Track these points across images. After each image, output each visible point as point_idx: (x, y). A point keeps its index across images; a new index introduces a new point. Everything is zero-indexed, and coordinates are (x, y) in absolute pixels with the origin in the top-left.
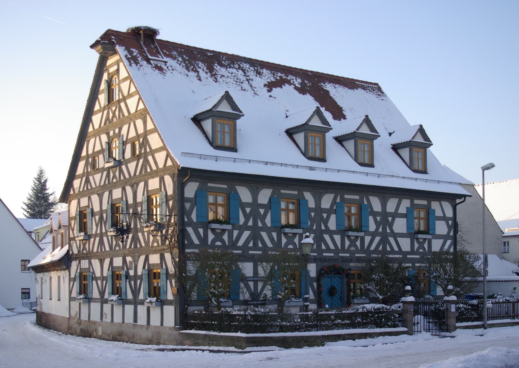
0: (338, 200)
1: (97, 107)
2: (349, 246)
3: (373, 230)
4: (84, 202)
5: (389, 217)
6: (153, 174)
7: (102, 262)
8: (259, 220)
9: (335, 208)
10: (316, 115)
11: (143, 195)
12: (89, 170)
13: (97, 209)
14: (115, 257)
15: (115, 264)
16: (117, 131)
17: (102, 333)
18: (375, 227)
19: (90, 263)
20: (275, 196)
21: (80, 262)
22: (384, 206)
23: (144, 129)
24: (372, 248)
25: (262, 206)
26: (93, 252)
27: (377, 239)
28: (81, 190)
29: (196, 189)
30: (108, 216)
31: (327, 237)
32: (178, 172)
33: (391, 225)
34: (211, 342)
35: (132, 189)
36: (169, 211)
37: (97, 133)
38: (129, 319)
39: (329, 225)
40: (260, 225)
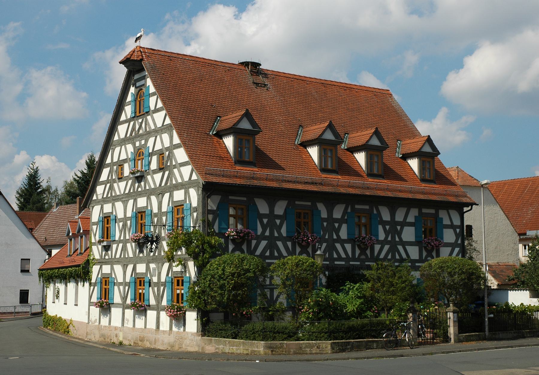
0: (349, 210)
1: (123, 118)
2: (360, 255)
3: (383, 239)
4: (107, 208)
5: (398, 226)
6: (178, 187)
7: (125, 267)
8: (275, 230)
9: (346, 218)
10: (328, 128)
11: (169, 205)
12: (114, 178)
13: (120, 215)
14: (138, 263)
15: (138, 271)
16: (143, 142)
17: (123, 338)
18: (384, 236)
19: (112, 269)
20: (290, 207)
21: (101, 268)
22: (393, 215)
23: (170, 143)
24: (382, 256)
25: (278, 217)
26: (115, 258)
27: (387, 247)
28: (105, 196)
29: (218, 202)
30: (132, 223)
31: (338, 246)
32: (203, 186)
33: (400, 234)
34: (231, 347)
35: (157, 199)
36: (193, 222)
37: (123, 142)
38: (151, 324)
39: (340, 234)
40: (276, 234)
